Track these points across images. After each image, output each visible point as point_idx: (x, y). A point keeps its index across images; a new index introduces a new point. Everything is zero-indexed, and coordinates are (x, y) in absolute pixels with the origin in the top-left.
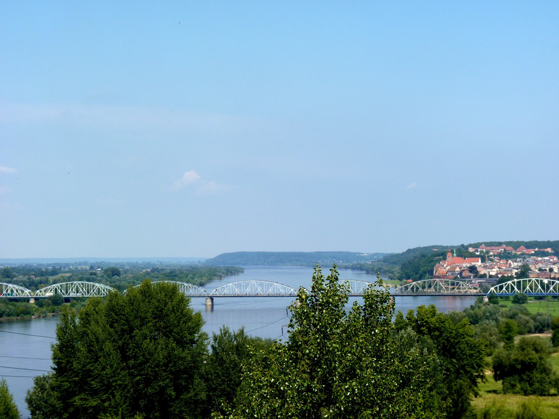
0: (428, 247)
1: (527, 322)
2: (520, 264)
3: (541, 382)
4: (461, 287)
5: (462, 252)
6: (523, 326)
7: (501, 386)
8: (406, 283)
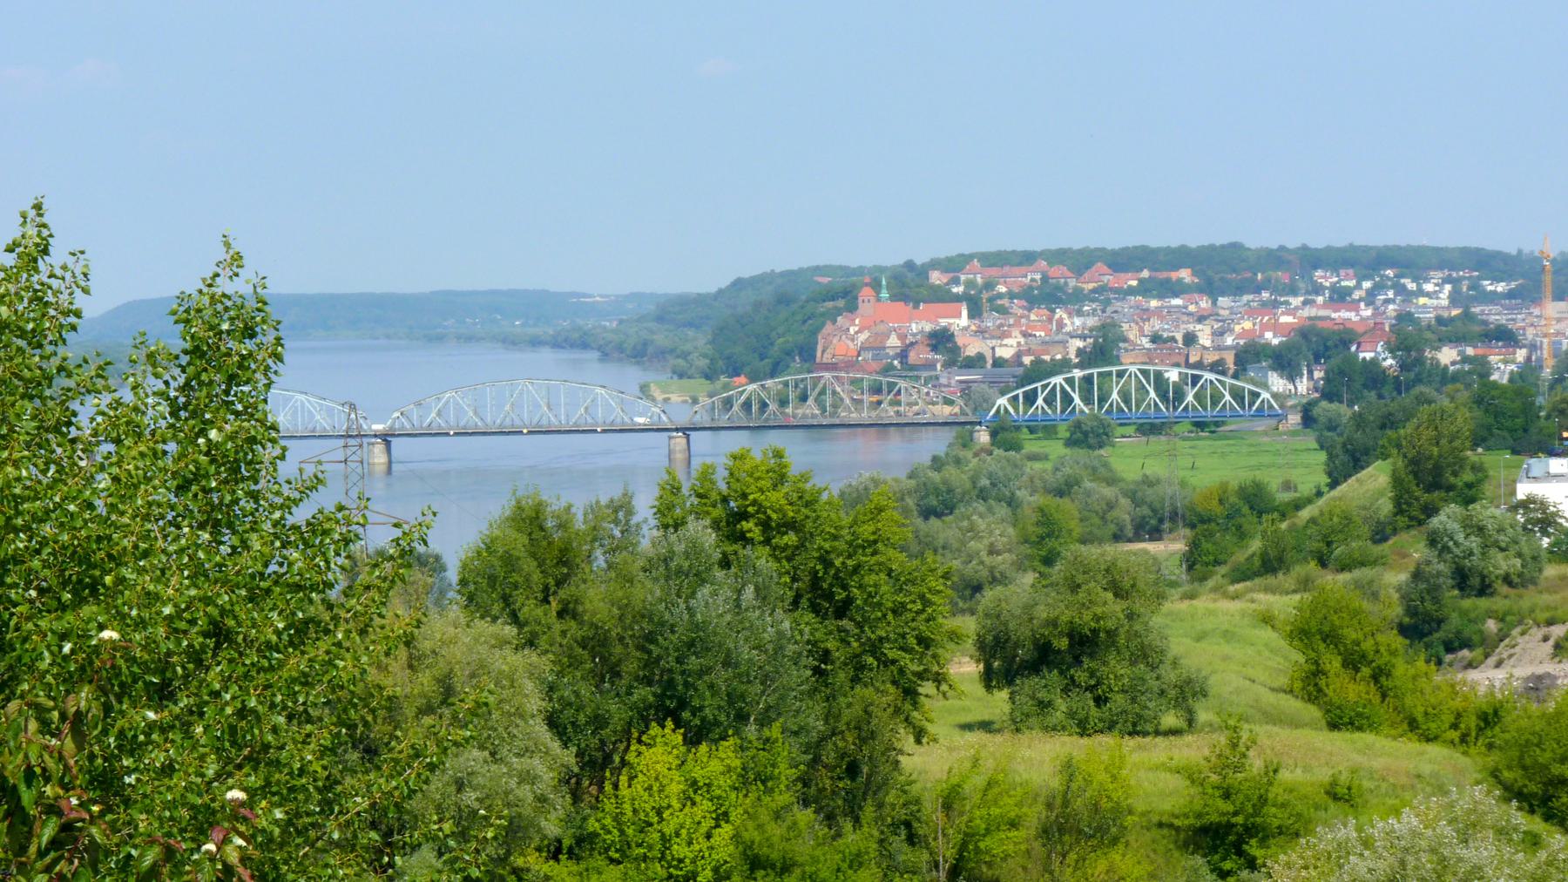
0: (801, 271)
1: (1111, 506)
2: (1092, 322)
3: (1133, 692)
4: (903, 397)
5: (909, 285)
6: (1096, 520)
7: (1007, 708)
8: (726, 387)
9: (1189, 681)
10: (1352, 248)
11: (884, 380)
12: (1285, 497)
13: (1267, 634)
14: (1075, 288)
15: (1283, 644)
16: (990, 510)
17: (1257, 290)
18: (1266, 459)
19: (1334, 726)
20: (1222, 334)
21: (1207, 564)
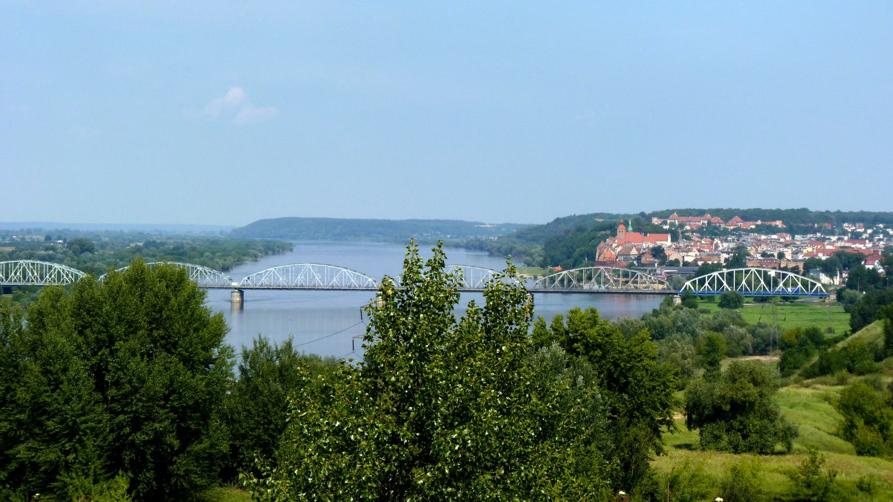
2: (732, 245)
3: (761, 433)
4: (639, 280)
5: (642, 224)
6: (734, 344)
7: (698, 438)
8: (551, 272)
9: (789, 429)
10: (862, 213)
11: (630, 271)
12: (828, 336)
13: (826, 406)
14: (724, 228)
15: (833, 410)
16: (683, 337)
17: (815, 232)
18: (819, 316)
19: (860, 453)
20: (797, 253)
21: (790, 368)
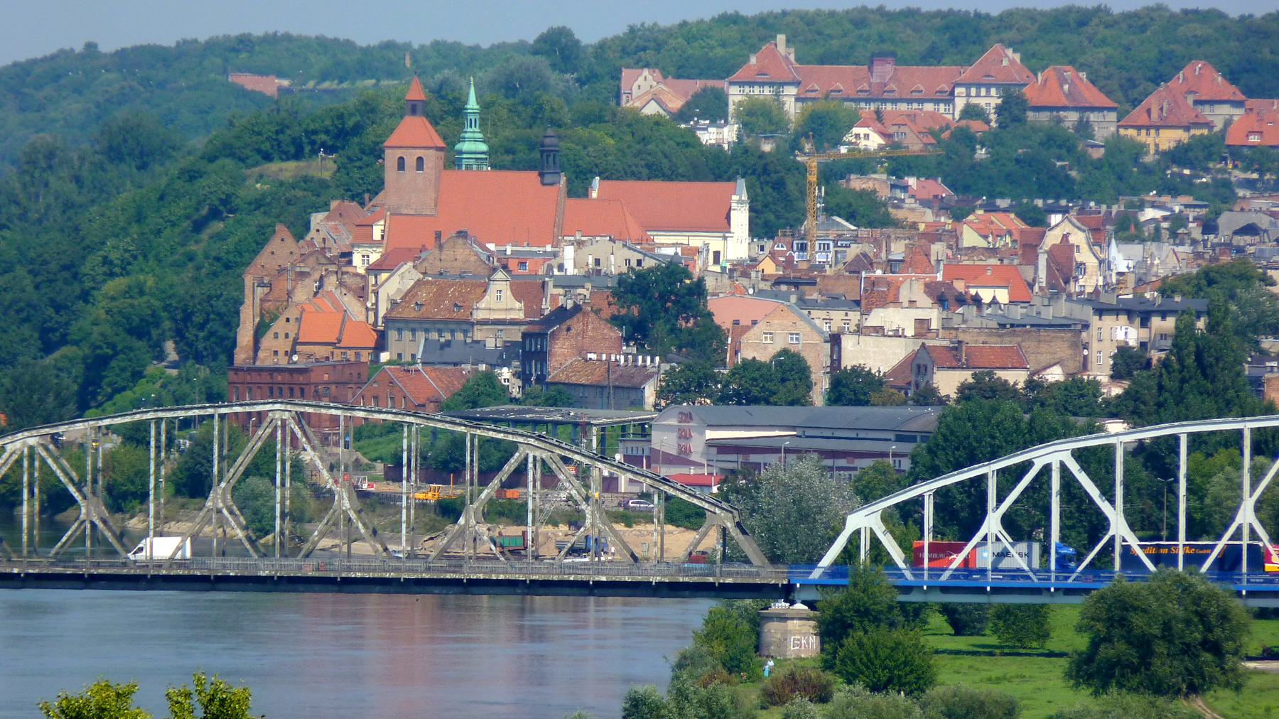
2: (1169, 260)
4: (531, 494)
5: (554, 118)
14: (1115, 146)
